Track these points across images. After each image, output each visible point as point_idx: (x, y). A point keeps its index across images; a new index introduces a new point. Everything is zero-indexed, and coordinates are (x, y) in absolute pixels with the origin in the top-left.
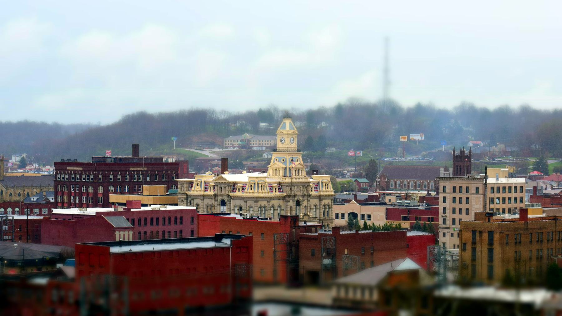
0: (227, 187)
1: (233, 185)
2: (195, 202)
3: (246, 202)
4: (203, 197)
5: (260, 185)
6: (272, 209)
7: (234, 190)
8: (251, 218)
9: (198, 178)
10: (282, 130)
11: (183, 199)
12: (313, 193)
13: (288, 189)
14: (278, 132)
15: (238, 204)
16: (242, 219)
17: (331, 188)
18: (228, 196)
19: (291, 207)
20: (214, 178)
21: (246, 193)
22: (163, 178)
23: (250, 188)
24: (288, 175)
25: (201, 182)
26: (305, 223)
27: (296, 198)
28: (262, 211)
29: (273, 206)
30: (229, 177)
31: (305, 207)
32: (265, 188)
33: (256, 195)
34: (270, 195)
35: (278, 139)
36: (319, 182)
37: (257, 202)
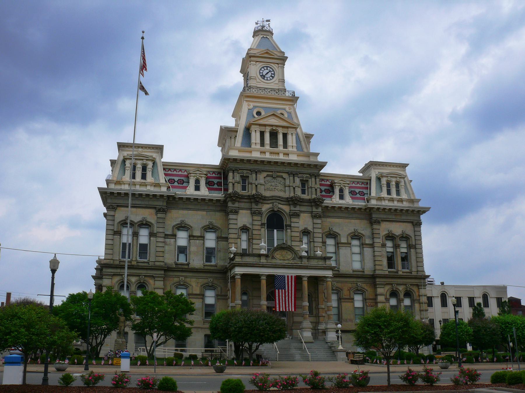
27: (265, 208)
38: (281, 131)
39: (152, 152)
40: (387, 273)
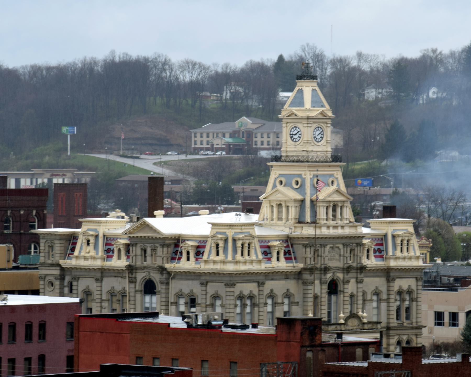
0: (159, 250)
1: (175, 244)
2: (82, 285)
3: (204, 284)
4: (102, 273)
5: (239, 244)
6: (269, 301)
7: (175, 256)
8: (208, 326)
9: (88, 226)
10: (294, 109)
11: (52, 279)
12: (372, 262)
13: (309, 253)
14: (284, 113)
15: (186, 291)
16: (185, 326)
17: (415, 251)
18: (162, 270)
19: (316, 297)
20: (128, 226)
21: (206, 262)
22: (7, 228)
23: (214, 251)
24: (308, 218)
25: (97, 237)
26: (340, 335)
27: (329, 276)
28: (244, 306)
29: (272, 295)
30: (164, 224)
31: (352, 296)
32: (252, 252)
33: (230, 267)
34: (264, 267)
35: (285, 132)
36: (385, 236)
37: (233, 285)
38: (340, 205)
39: (384, 226)
40: (396, 325)
